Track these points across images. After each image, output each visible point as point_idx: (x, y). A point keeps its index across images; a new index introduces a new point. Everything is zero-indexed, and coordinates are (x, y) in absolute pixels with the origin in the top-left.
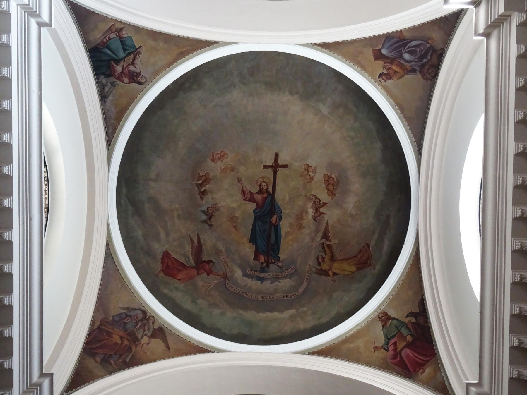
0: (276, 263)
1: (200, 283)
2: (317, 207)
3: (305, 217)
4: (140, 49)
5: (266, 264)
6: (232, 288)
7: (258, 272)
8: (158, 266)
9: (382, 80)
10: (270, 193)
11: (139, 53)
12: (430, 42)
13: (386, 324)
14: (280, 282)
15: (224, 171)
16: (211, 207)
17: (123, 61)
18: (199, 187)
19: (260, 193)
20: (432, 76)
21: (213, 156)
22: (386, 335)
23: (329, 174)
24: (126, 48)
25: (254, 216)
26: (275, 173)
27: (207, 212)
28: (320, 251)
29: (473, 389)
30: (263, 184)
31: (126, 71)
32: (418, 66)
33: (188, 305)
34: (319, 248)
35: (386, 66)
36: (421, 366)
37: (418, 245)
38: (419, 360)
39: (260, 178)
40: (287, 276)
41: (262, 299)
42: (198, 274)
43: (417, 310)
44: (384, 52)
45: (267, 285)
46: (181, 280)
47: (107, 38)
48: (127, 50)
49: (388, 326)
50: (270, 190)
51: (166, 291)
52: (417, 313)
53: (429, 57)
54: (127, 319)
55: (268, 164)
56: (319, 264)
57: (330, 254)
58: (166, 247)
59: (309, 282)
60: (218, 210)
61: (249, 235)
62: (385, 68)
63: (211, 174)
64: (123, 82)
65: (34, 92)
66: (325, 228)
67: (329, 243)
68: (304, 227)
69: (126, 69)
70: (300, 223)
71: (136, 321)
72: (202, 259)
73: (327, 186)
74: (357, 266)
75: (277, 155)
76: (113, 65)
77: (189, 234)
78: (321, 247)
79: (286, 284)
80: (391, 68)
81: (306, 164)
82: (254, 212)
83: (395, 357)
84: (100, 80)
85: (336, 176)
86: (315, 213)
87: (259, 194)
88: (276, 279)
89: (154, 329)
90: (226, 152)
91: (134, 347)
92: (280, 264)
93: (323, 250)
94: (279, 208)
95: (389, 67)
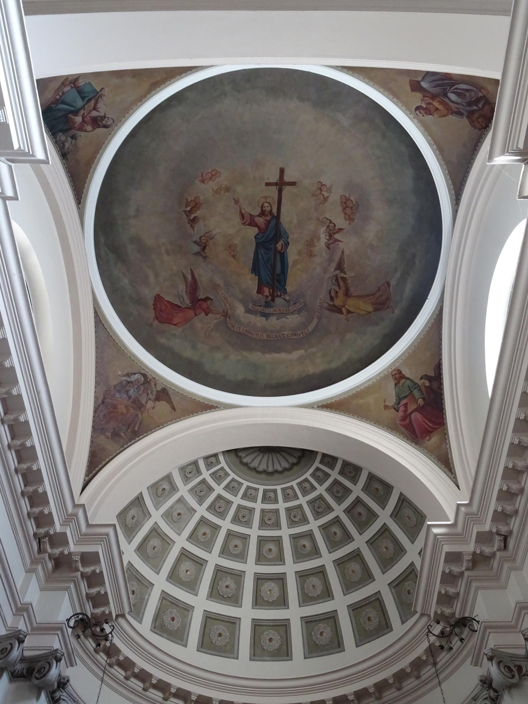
0: (282, 297)
1: (199, 325)
2: (331, 233)
3: (316, 244)
4: (102, 91)
5: (272, 297)
6: (234, 327)
7: (263, 307)
8: (151, 314)
9: (420, 114)
10: (275, 215)
11: (101, 96)
12: (483, 91)
13: (399, 382)
14: (287, 318)
15: (217, 192)
16: (204, 236)
17: (83, 110)
18: (188, 214)
19: (261, 215)
20: (482, 126)
21: (202, 175)
22: (398, 395)
23: (347, 196)
24: (84, 95)
25: (256, 243)
26: (280, 192)
27: (200, 242)
28: (333, 284)
29: (463, 509)
30: (266, 205)
31: (88, 119)
32: (466, 111)
33: (188, 353)
34: (332, 281)
35: (425, 100)
36: (428, 433)
37: (442, 304)
38: (426, 426)
39: (262, 197)
40: (295, 310)
41: (268, 339)
42: (196, 315)
43: (432, 374)
44: (423, 84)
45: (273, 322)
46: (177, 325)
47: (60, 94)
48: (86, 97)
49: (400, 385)
50: (275, 211)
51: (163, 341)
52: (432, 377)
53: (480, 105)
54: (128, 386)
55: (271, 181)
56: (332, 298)
57: (344, 289)
58: (156, 292)
59: (320, 319)
60: (212, 238)
61: (251, 266)
62: (423, 102)
63: (201, 198)
64: (86, 131)
65: (14, 275)
66: (340, 258)
67: (345, 276)
68: (315, 255)
69: (88, 116)
70: (311, 251)
71: (138, 386)
72: (199, 297)
73: (344, 209)
74: (373, 306)
75: (282, 171)
76: (71, 118)
77: (182, 271)
78: (334, 281)
79: (294, 320)
80: (432, 104)
81: (319, 182)
82: (255, 238)
83: (404, 419)
84: (58, 138)
85: (355, 199)
86: (328, 240)
87: (261, 217)
88: (281, 315)
89: (157, 391)
90: (218, 170)
91: (140, 414)
92: (287, 298)
93: (336, 283)
94: (286, 232)
95: (429, 102)
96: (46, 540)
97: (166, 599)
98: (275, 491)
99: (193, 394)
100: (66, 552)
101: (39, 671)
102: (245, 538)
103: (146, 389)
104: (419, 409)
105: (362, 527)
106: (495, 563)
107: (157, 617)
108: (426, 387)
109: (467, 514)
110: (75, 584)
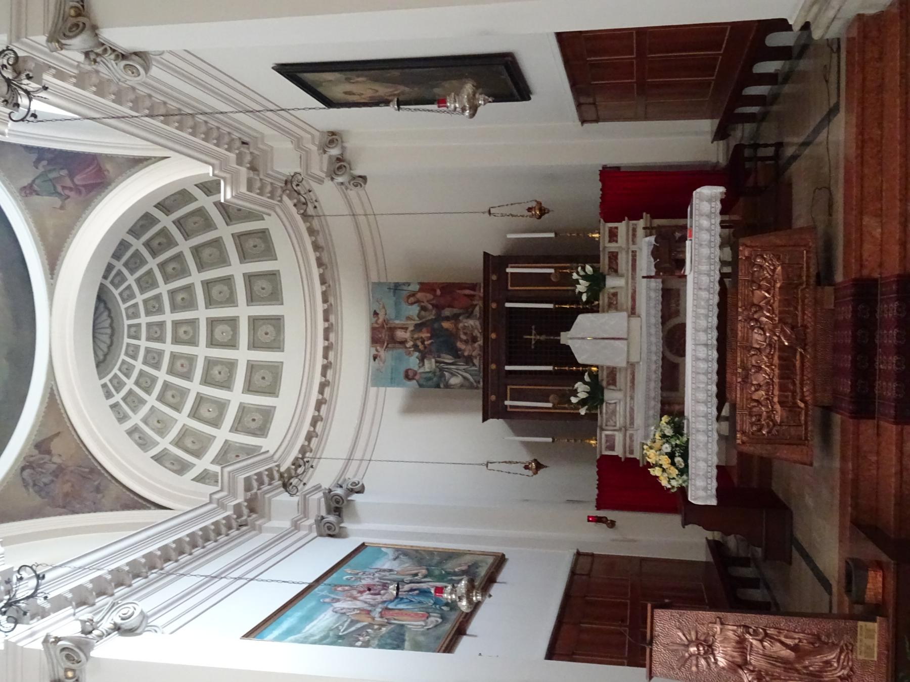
13: (35, 191)
22: (50, 194)
83: (79, 192)
96: (239, 520)
97: (237, 428)
98: (130, 326)
99: (37, 416)
100: (246, 504)
101: (338, 502)
102: (174, 356)
103: (41, 466)
104: (71, 176)
105: (171, 243)
106: (256, 152)
107: (253, 434)
108: (48, 164)
109: (221, 170)
110: (266, 494)
